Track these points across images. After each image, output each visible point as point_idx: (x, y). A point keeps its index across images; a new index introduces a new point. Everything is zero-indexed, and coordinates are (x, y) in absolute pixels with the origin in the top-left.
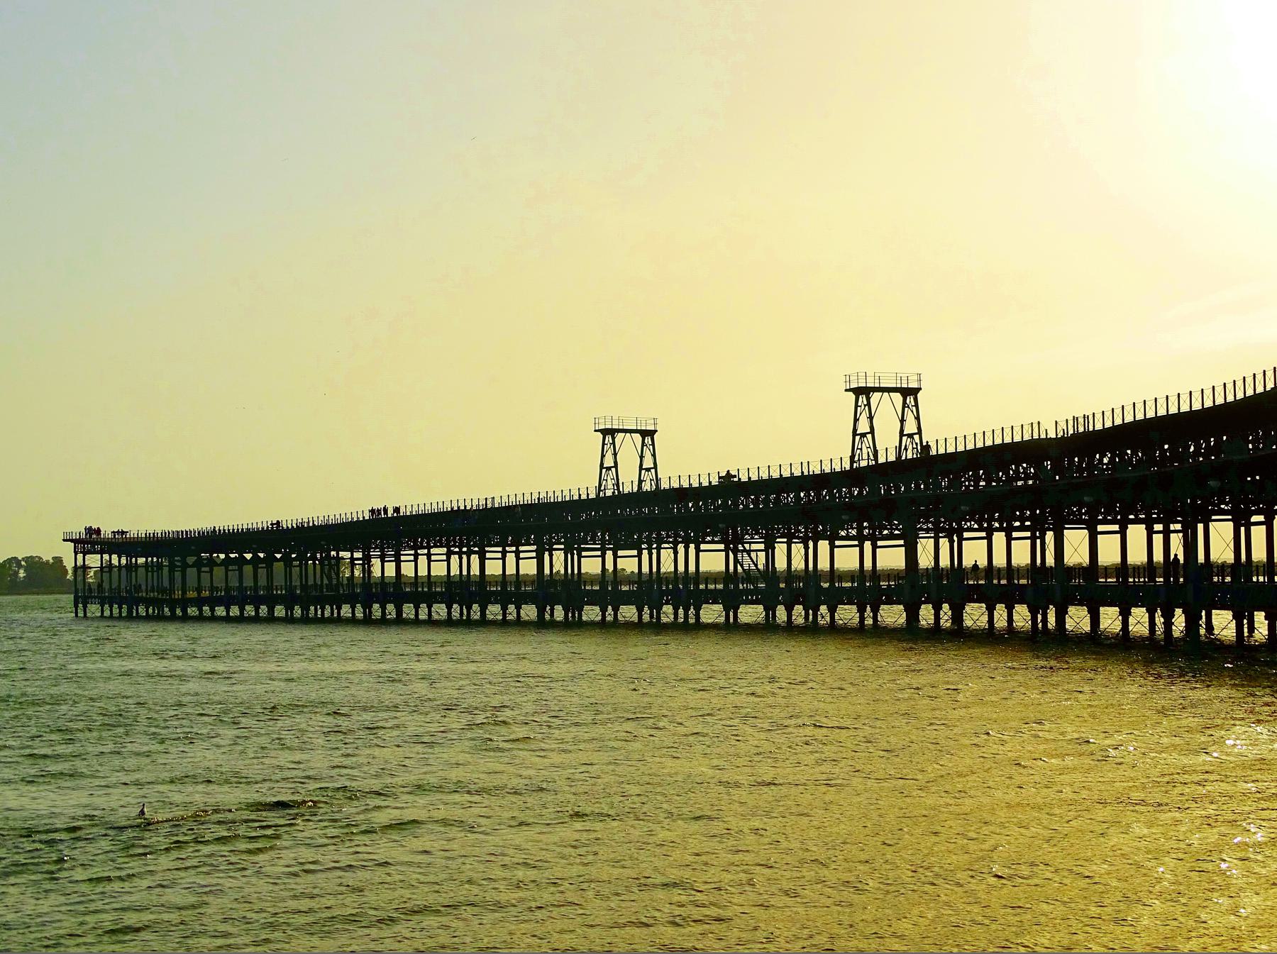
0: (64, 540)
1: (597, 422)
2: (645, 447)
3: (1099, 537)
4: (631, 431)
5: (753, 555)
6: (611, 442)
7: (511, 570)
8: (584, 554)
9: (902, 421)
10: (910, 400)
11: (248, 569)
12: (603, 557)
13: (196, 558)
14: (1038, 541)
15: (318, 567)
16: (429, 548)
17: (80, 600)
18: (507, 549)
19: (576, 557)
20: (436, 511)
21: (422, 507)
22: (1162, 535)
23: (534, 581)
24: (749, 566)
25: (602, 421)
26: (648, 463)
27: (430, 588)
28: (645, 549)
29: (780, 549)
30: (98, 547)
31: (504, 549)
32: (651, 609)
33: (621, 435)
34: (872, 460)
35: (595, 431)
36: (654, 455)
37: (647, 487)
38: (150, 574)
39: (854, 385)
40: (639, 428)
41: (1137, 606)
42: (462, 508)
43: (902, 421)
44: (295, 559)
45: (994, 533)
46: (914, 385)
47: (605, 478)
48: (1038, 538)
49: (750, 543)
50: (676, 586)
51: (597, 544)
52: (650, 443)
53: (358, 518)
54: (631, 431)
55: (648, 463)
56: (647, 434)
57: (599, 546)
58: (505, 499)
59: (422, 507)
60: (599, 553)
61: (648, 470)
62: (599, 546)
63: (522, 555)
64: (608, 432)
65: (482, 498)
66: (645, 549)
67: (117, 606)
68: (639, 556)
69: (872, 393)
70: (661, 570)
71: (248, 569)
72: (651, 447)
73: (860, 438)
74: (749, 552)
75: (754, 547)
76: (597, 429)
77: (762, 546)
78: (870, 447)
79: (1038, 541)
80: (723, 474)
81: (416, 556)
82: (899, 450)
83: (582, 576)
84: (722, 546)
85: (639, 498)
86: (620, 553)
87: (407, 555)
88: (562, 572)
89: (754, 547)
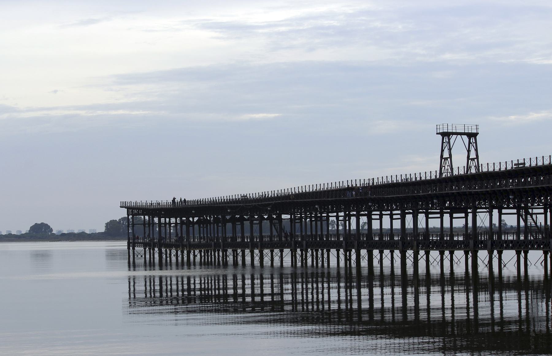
0: (121, 207)
1: (438, 127)
2: (471, 144)
3: (373, 221)
4: (461, 134)
5: (534, 216)
6: (447, 141)
7: (447, 224)
8: (430, 216)
9: (469, 151)
10: (473, 140)
11: (229, 225)
12: (442, 218)
13: (198, 218)
14: (347, 222)
15: (314, 223)
16: (391, 211)
17: (131, 245)
18: (383, 212)
19: (216, 226)
20: (386, 183)
21: (330, 186)
22: (400, 220)
23: (412, 233)
24: (531, 224)
25: (441, 127)
26: (473, 155)
27: (327, 238)
28: (470, 212)
29: (421, 217)
30: (140, 212)
31: (381, 213)
32: (302, 251)
33: (454, 136)
34: (450, 173)
35: (437, 134)
36: (476, 150)
37: (473, 171)
38: (202, 229)
39: (441, 131)
40: (466, 131)
41: (333, 248)
42: (350, 186)
43: (469, 151)
44: (256, 220)
45: (419, 214)
46: (474, 131)
47: (444, 165)
48: (347, 220)
49: (532, 209)
50: (442, 237)
51: (438, 209)
52: (474, 142)
53: (352, 185)
54: (461, 134)
55: (473, 155)
56: (472, 136)
57: (439, 211)
58: (334, 185)
59: (380, 180)
60: (439, 215)
61: (473, 159)
62: (439, 211)
63: (394, 217)
64: (446, 135)
65: (366, 179)
66: (470, 212)
67: (157, 249)
68: (466, 217)
69: (451, 135)
70: (273, 234)
71: (229, 225)
72: (474, 144)
73: (444, 160)
74: (531, 215)
75: (535, 211)
76: (438, 132)
77: (542, 211)
78: (449, 166)
79: (347, 222)
80: (242, 195)
81: (381, 216)
82: (468, 168)
83: (521, 228)
84: (515, 211)
85: (466, 178)
86: (455, 215)
87: (375, 215)
88: (543, 224)
89: (535, 211)
